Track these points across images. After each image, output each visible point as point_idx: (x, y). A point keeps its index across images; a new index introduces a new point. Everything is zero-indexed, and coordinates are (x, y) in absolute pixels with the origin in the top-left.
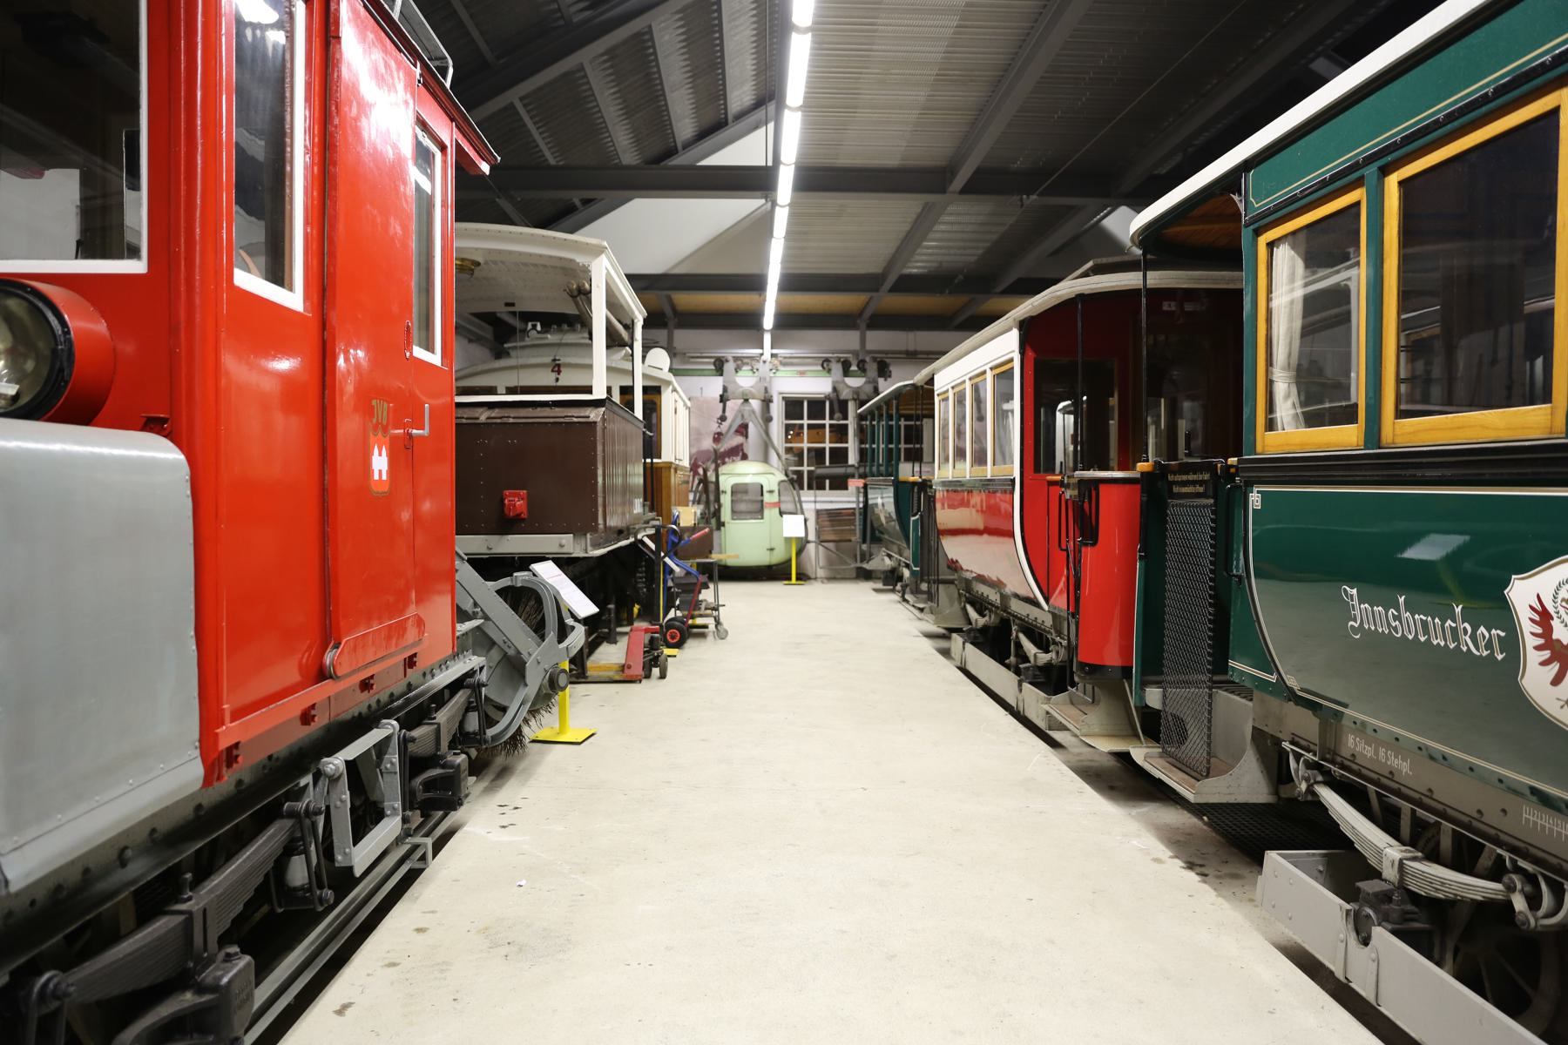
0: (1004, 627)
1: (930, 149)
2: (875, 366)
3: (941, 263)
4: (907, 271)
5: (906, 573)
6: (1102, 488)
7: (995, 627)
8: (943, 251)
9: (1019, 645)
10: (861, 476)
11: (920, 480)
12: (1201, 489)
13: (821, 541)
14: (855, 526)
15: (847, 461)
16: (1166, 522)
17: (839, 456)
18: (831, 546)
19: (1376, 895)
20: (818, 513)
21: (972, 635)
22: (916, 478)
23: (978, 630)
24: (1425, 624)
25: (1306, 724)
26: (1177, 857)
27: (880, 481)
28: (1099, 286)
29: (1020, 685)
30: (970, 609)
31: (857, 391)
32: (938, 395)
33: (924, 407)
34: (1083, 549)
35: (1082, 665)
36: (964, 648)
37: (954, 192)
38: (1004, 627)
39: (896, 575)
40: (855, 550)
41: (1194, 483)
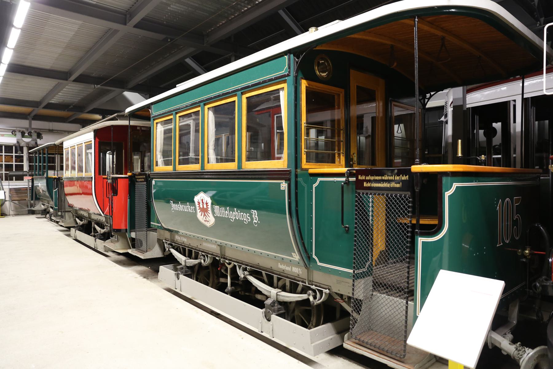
0: (90, 223)
1: (63, 65)
2: (36, 134)
3: (64, 100)
4: (50, 102)
5: (51, 210)
6: (118, 180)
7: (86, 224)
8: (65, 97)
9: (95, 229)
10: (30, 176)
11: (57, 177)
12: (143, 180)
13: (12, 200)
14: (27, 194)
15: (23, 170)
16: (135, 189)
17: (20, 168)
18: (16, 202)
19: (180, 268)
20: (10, 190)
21: (78, 227)
22: (56, 176)
23: (80, 226)
24: (183, 207)
25: (167, 235)
26: (141, 276)
27: (38, 177)
28: (118, 124)
29: (95, 240)
30: (77, 219)
31: (28, 144)
32: (65, 149)
33: (59, 151)
34: (113, 197)
35: (114, 230)
36: (75, 232)
37: (71, 81)
38: (90, 223)
39: (46, 211)
40: (28, 203)
41: (142, 178)
